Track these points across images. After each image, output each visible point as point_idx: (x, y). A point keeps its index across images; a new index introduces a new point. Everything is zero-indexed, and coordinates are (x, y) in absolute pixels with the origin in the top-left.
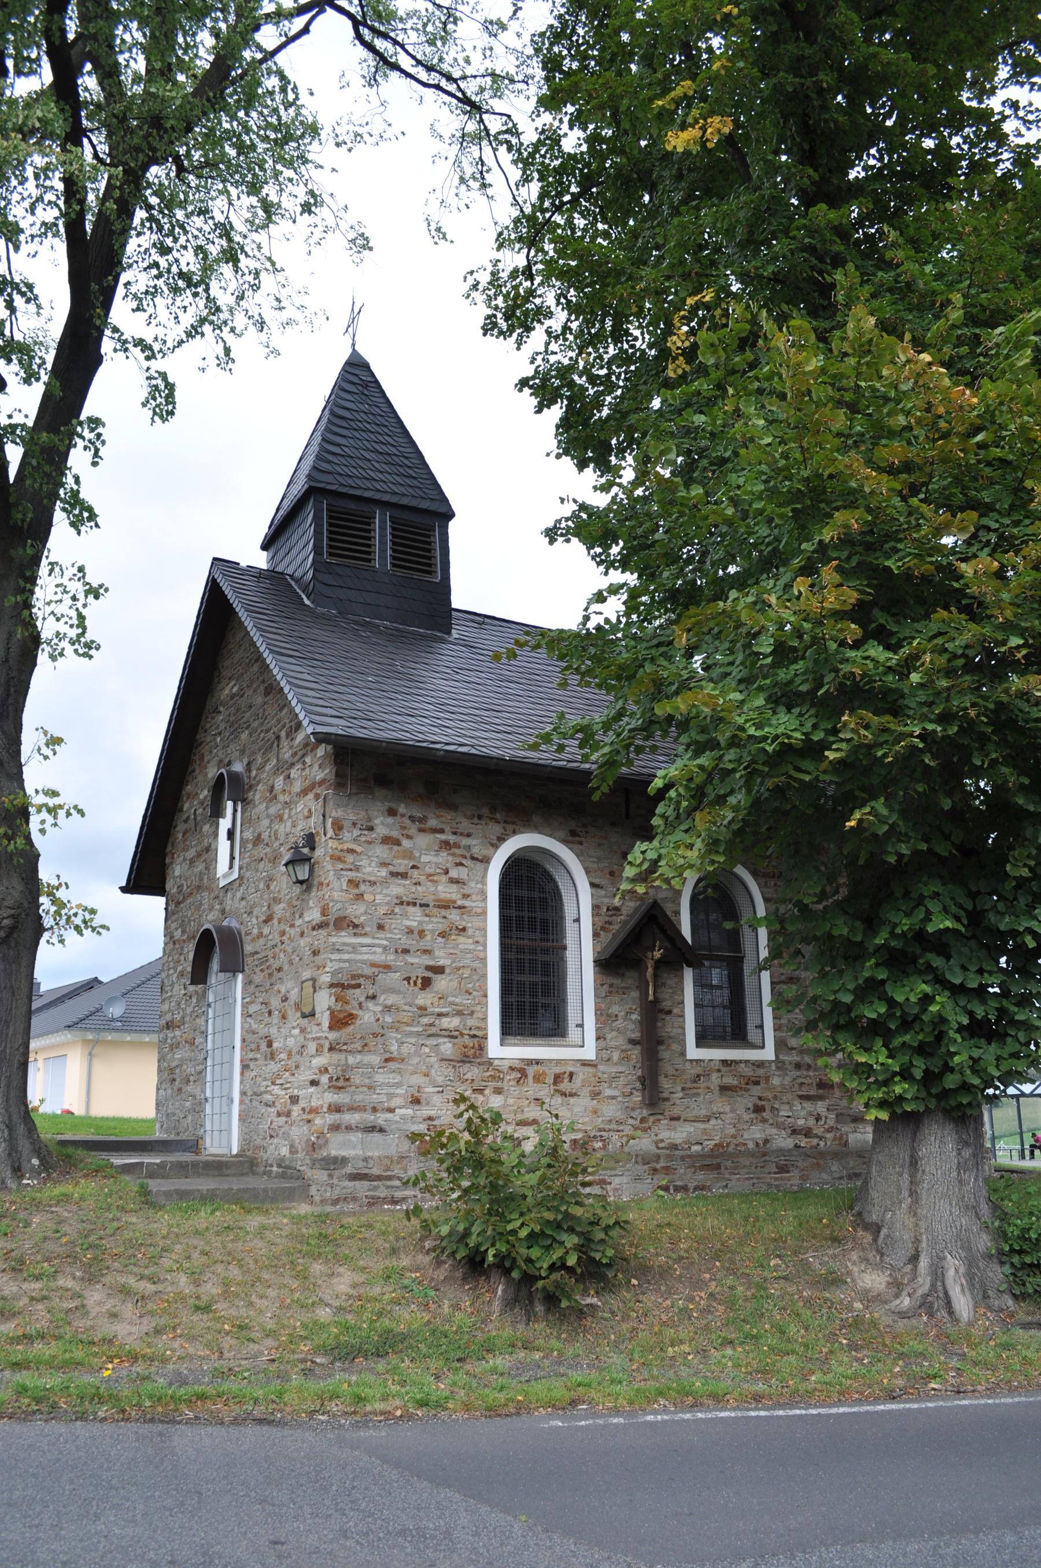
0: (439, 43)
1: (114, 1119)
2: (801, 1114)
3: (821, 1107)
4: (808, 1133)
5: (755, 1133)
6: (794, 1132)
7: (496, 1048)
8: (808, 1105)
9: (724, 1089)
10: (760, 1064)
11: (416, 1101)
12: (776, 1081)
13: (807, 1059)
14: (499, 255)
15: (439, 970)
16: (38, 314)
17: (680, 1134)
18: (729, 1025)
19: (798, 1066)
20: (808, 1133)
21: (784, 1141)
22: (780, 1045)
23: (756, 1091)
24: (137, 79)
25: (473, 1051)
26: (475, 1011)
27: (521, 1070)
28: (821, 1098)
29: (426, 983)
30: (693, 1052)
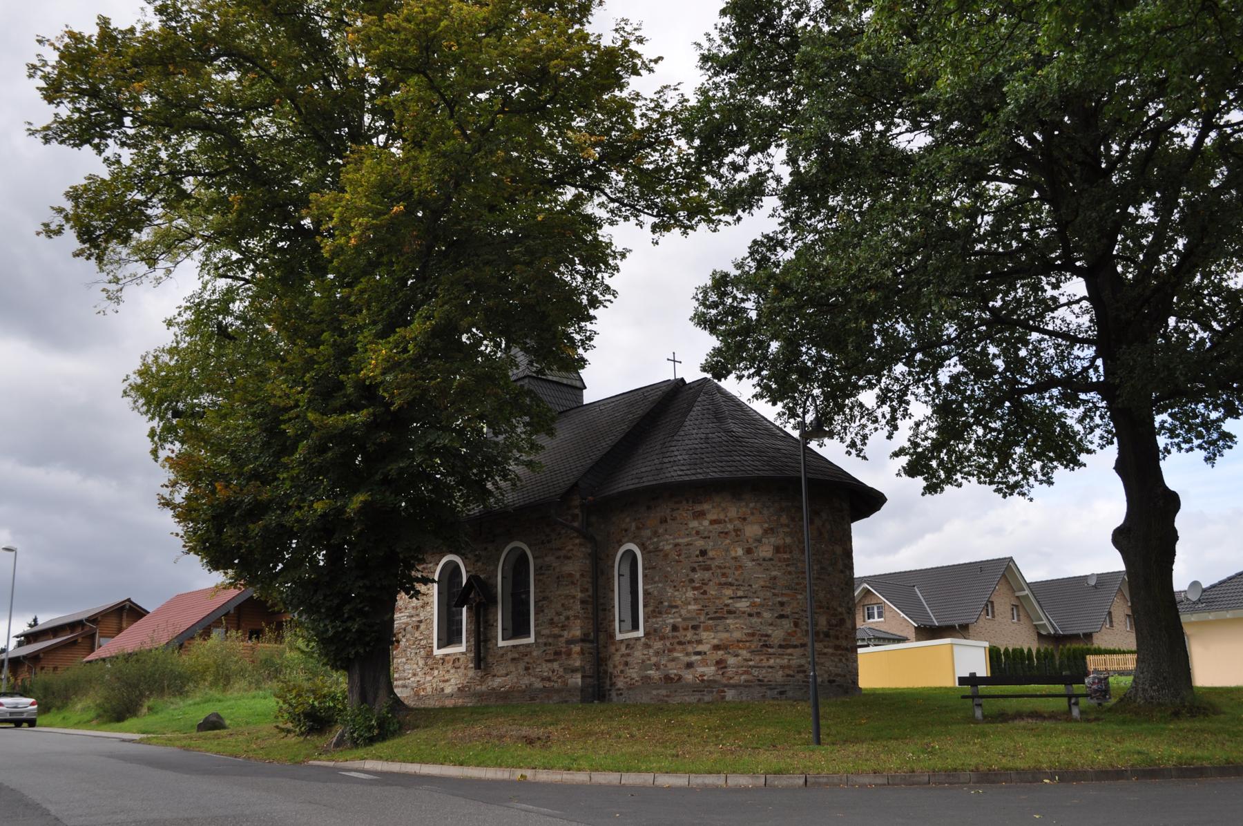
0: (987, 117)
1: (936, 688)
2: (545, 669)
3: (555, 665)
4: (549, 679)
5: (526, 681)
6: (543, 679)
7: (437, 652)
8: (549, 665)
9: (513, 659)
10: (528, 645)
11: (414, 675)
12: (535, 654)
13: (550, 640)
14: (104, 155)
15: (421, 622)
16: (890, 437)
17: (497, 682)
18: (518, 627)
19: (545, 644)
20: (549, 679)
21: (538, 684)
22: (537, 634)
23: (526, 659)
24: (247, 243)
25: (430, 655)
26: (430, 637)
27: (444, 659)
28: (555, 660)
29: (418, 627)
30: (501, 643)
